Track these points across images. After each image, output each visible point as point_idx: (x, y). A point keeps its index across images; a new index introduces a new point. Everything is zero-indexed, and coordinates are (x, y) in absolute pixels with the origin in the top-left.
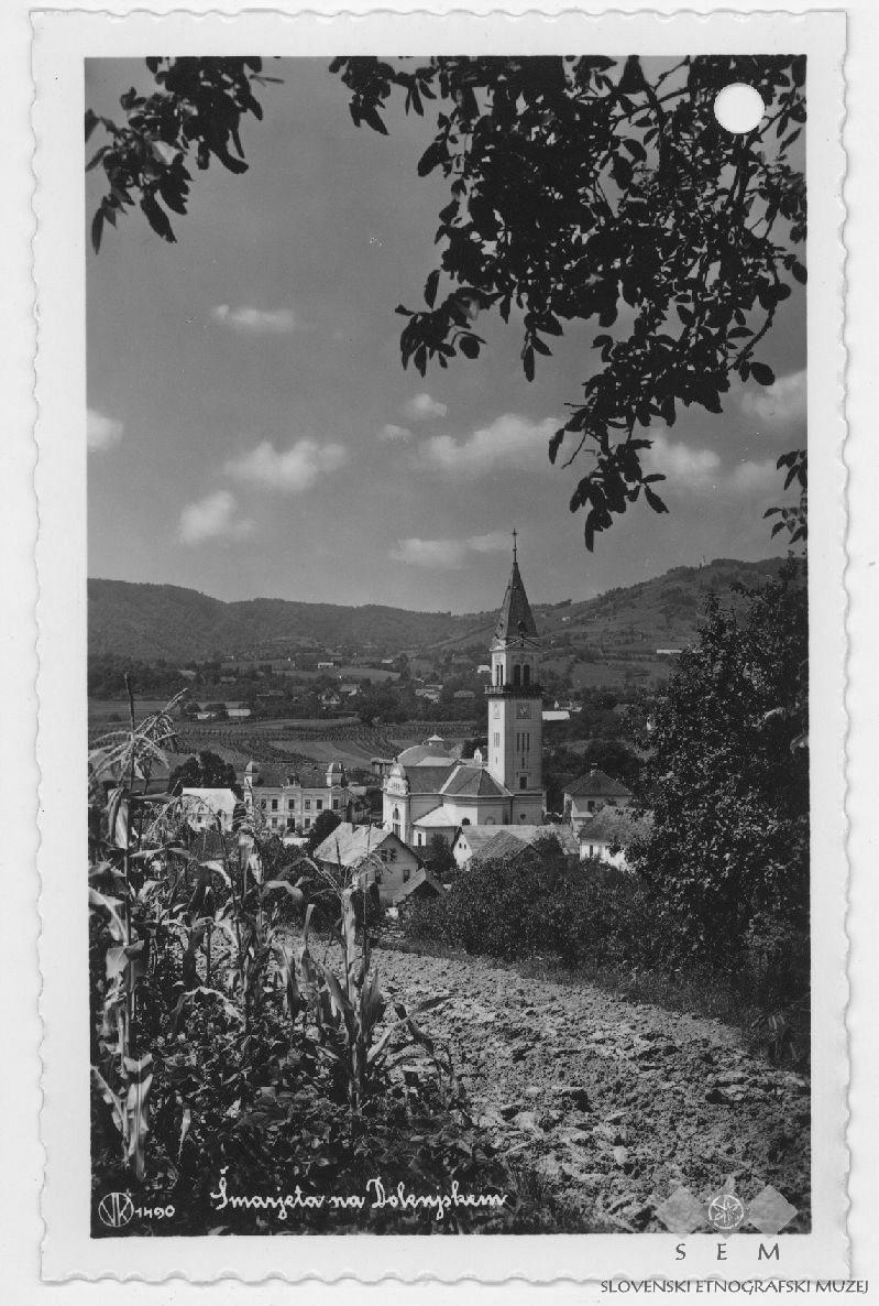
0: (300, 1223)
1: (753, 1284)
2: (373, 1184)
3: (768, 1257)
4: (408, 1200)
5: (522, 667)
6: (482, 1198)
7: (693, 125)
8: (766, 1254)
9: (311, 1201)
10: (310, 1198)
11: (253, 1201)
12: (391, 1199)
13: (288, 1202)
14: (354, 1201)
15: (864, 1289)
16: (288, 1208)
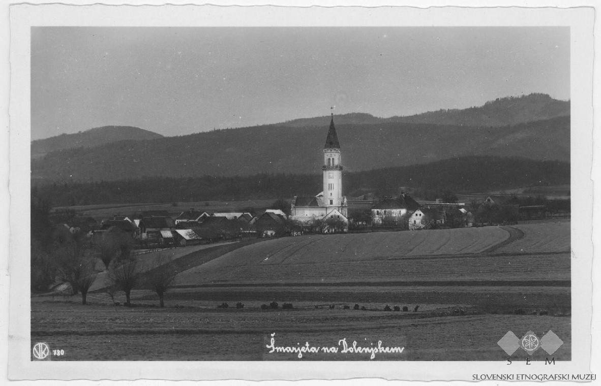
15: (594, 378)
16: (302, 352)
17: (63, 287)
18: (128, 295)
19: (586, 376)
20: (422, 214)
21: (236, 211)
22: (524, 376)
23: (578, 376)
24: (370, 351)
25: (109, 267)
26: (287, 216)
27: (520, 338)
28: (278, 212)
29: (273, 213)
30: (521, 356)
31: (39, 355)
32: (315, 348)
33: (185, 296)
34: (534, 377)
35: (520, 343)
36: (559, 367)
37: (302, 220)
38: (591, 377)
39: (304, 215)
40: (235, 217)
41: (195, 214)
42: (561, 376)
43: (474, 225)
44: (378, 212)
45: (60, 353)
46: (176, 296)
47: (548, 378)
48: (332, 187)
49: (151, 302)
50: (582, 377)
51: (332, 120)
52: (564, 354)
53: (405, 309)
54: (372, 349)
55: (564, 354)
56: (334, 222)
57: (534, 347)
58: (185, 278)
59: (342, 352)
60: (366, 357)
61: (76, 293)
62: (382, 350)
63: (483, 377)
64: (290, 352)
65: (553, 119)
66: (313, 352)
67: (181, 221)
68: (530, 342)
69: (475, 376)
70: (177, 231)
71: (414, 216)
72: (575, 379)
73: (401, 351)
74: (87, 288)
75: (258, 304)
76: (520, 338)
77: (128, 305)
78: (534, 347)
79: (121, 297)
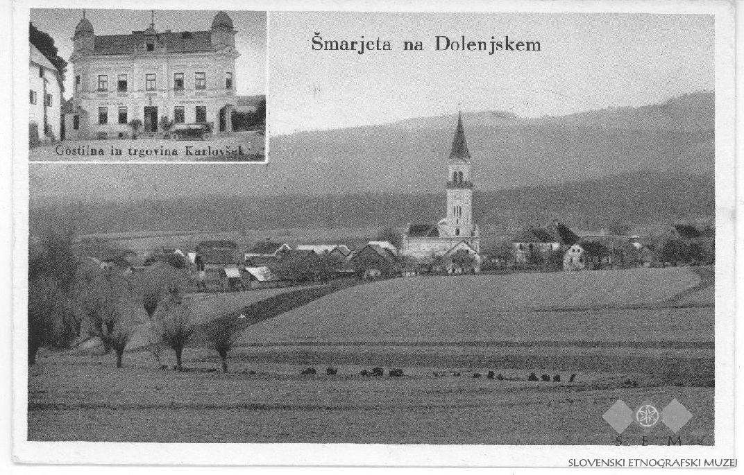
17: (90, 344)
18: (179, 355)
19: (724, 462)
20: (582, 250)
21: (328, 243)
22: (639, 462)
23: (712, 461)
25: (154, 318)
26: (398, 251)
28: (385, 244)
29: (378, 246)
30: (635, 436)
33: (253, 358)
34: (653, 463)
37: (418, 256)
39: (417, 249)
40: (326, 251)
41: (273, 246)
42: (690, 462)
43: (652, 266)
44: (521, 246)
46: (244, 358)
47: (671, 463)
49: (209, 366)
50: (718, 463)
51: (460, 119)
53: (557, 378)
56: (462, 260)
57: (652, 422)
58: (250, 337)
61: (108, 351)
63: (583, 463)
65: (687, 125)
67: (252, 255)
68: (647, 415)
69: (573, 462)
70: (247, 269)
71: (570, 252)
72: (709, 465)
74: (124, 345)
75: (356, 369)
77: (179, 368)
78: (652, 422)
79: (168, 356)
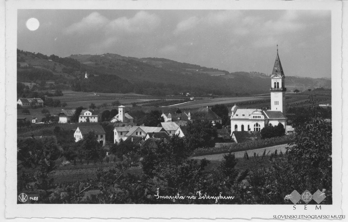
0: (179, 202)
1: (314, 216)
2: (198, 193)
3: (318, 209)
4: (208, 197)
5: (277, 83)
6: (228, 197)
7: (104, 147)
8: (318, 208)
9: (182, 197)
10: (181, 196)
11: (166, 197)
12: (203, 197)
13: (176, 197)
14: (193, 197)
15: (344, 217)
16: (175, 199)
22: (303, 216)
23: (335, 216)
24: (214, 198)
27: (301, 194)
31: (22, 200)
32: (182, 197)
34: (309, 217)
35: (301, 197)
36: (325, 207)
38: (342, 217)
42: (325, 216)
45: (36, 198)
47: (317, 217)
48: (276, 103)
50: (337, 217)
52: (328, 201)
54: (216, 197)
55: (328, 201)
57: (309, 199)
59: (199, 198)
60: (212, 202)
62: (221, 197)
63: (279, 217)
64: (168, 198)
66: (182, 198)
69: (275, 216)
72: (333, 218)
73: (233, 198)
76: (301, 194)
78: (309, 199)
